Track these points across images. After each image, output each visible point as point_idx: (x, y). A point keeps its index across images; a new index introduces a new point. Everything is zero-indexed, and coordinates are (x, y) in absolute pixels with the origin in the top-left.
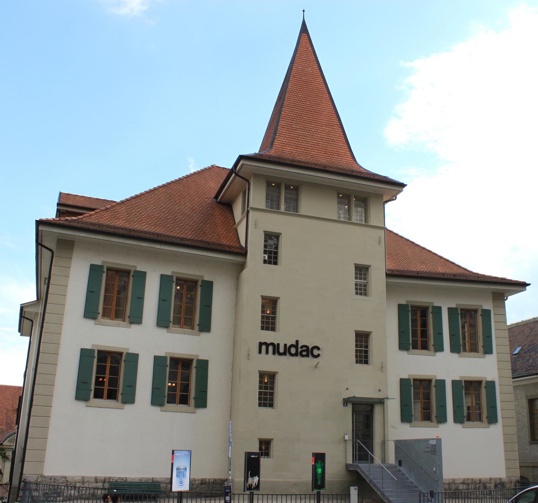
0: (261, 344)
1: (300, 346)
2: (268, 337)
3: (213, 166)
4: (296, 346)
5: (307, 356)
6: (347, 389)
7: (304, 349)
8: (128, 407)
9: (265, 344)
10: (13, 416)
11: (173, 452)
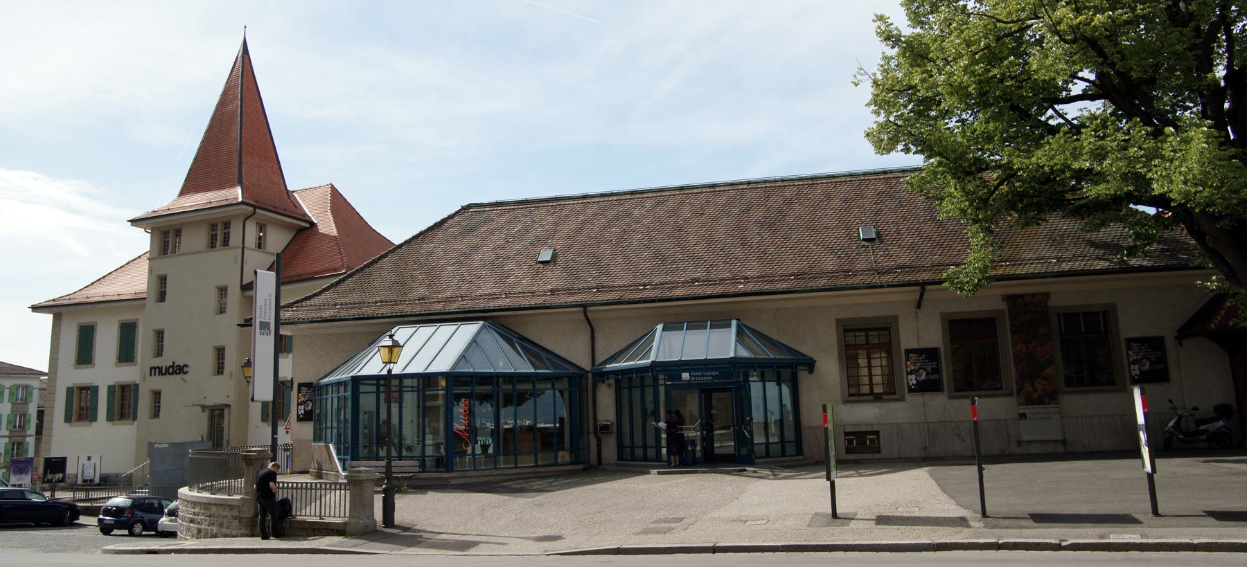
0: (151, 368)
1: (175, 365)
2: (157, 362)
3: (1144, 212)
4: (172, 367)
5: (180, 373)
6: (205, 397)
7: (178, 367)
8: (93, 424)
9: (154, 367)
10: (955, 163)
11: (162, 297)
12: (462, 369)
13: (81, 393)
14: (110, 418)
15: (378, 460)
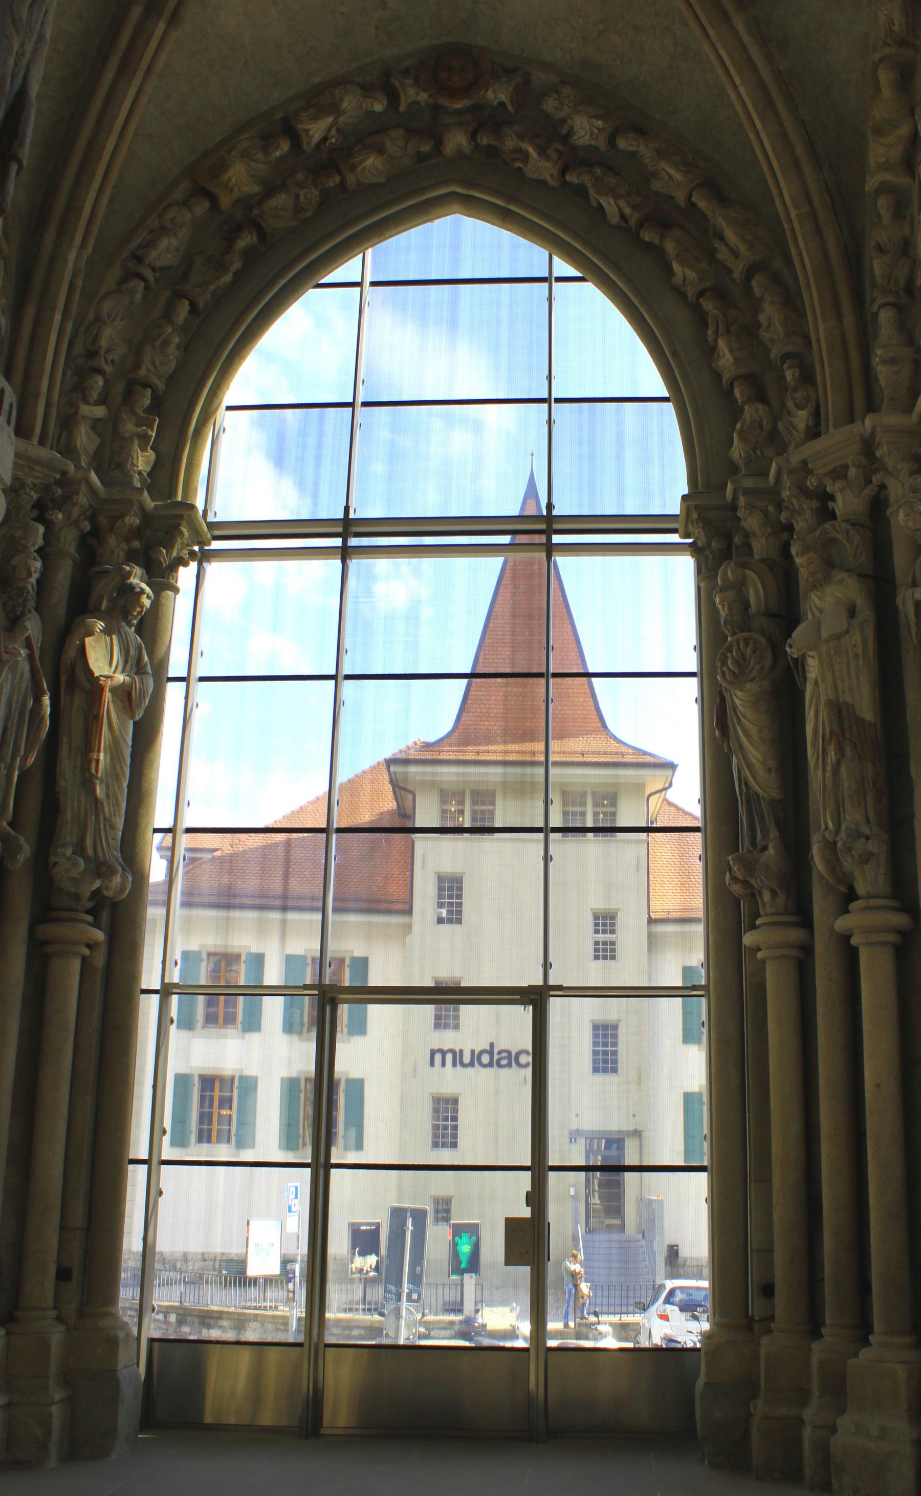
1: (496, 1051)
4: (490, 1052)
12: (306, 838)
13: (171, 379)
14: (249, 1085)
15: (772, 1251)
